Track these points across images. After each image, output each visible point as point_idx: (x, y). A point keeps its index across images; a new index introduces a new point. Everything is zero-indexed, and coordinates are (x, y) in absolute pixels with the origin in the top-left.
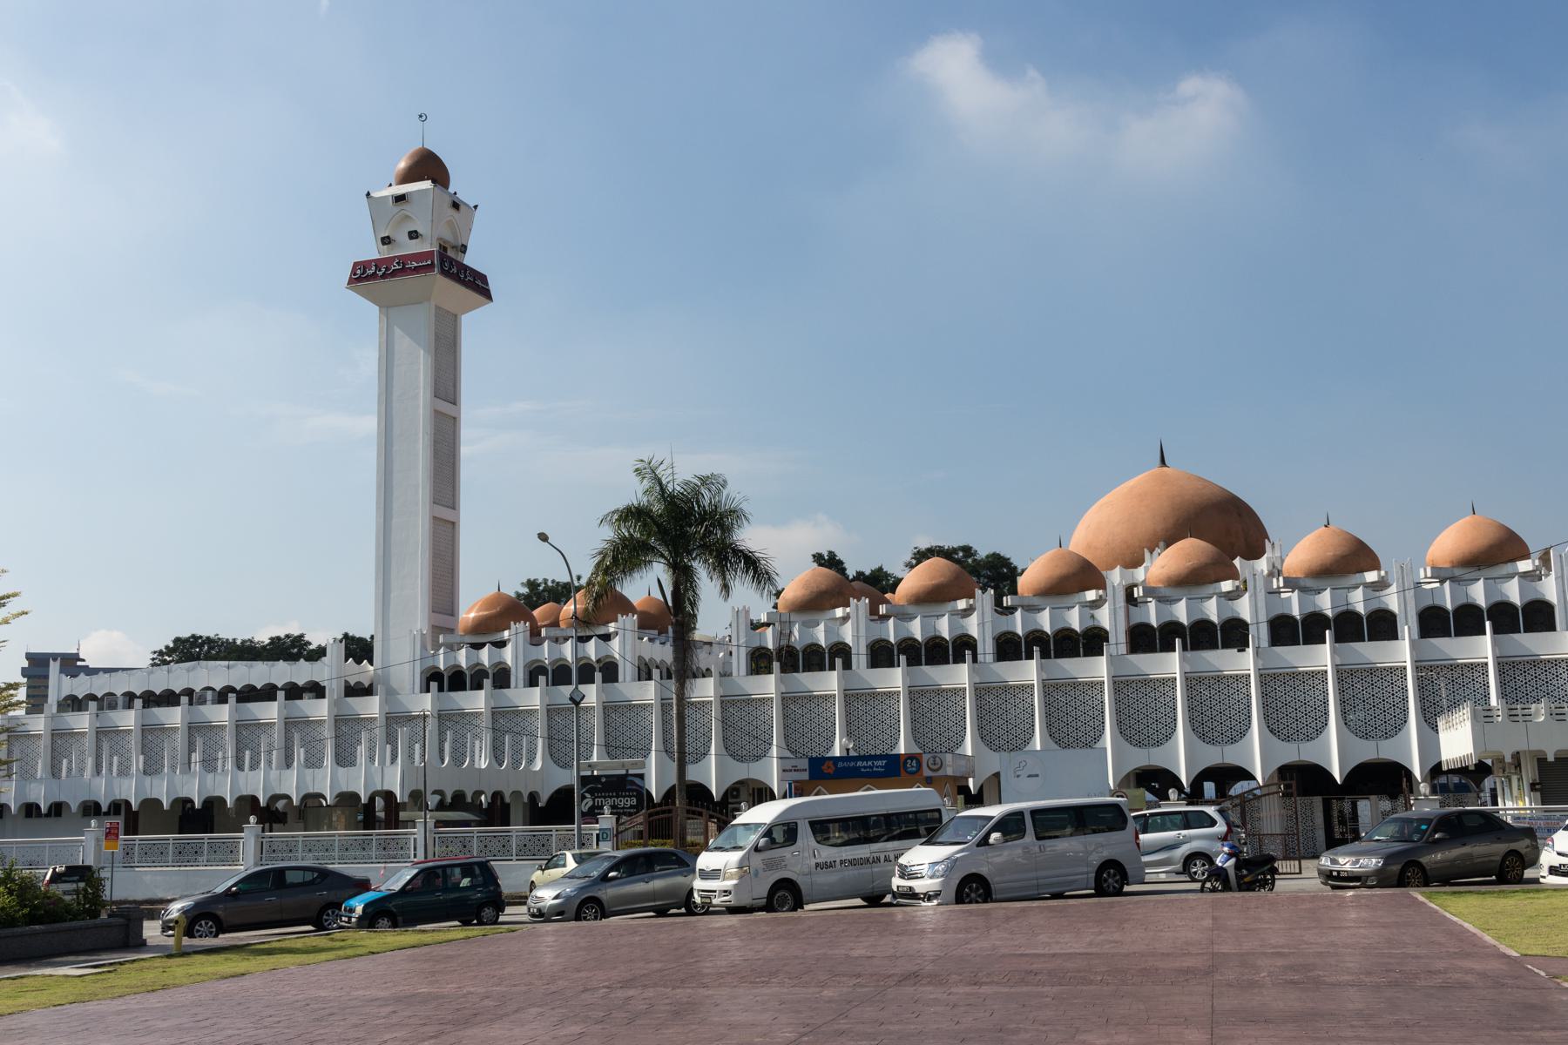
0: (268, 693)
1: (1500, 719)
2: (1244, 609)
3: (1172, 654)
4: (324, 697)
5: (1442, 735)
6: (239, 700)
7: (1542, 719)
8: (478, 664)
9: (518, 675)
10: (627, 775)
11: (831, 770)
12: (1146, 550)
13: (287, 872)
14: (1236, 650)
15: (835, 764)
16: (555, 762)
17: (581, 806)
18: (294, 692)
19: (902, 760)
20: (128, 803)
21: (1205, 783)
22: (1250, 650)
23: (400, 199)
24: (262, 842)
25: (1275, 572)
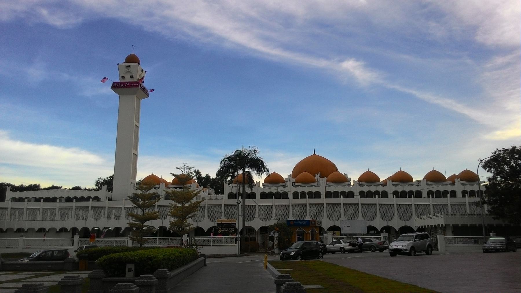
2: (319, 189)
24: (79, 241)
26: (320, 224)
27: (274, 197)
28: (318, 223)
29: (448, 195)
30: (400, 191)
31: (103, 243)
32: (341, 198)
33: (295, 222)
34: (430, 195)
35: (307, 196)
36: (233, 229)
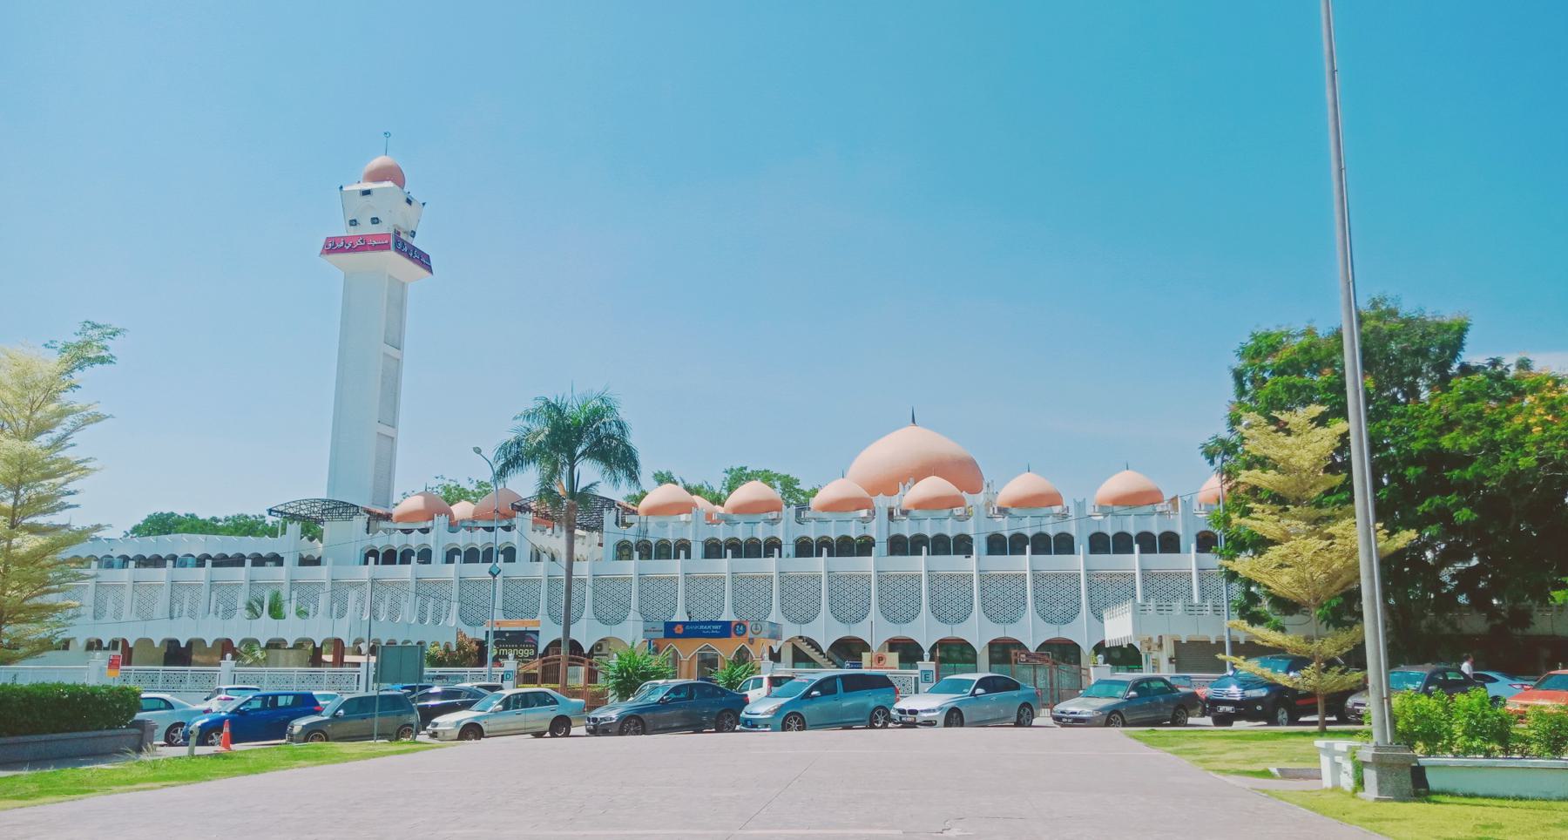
0: (238, 561)
1: (1208, 613)
2: (970, 529)
3: (920, 557)
4: (282, 565)
5: (1106, 622)
6: (214, 565)
7: (1179, 613)
8: (407, 545)
9: (438, 555)
10: (526, 632)
11: (681, 632)
12: (900, 483)
13: (279, 697)
14: (964, 556)
15: (684, 627)
16: (463, 621)
17: (492, 652)
18: (259, 561)
19: (733, 625)
20: (125, 641)
21: (863, 654)
22: (974, 557)
23: (367, 193)
25: (989, 504)
26: (737, 635)
27: (1028, 548)
28: (755, 631)
29: (1027, 547)
30: (1157, 532)
31: (160, 681)
32: (725, 557)
33: (687, 627)
34: (825, 550)
35: (1136, 547)
36: (532, 648)
